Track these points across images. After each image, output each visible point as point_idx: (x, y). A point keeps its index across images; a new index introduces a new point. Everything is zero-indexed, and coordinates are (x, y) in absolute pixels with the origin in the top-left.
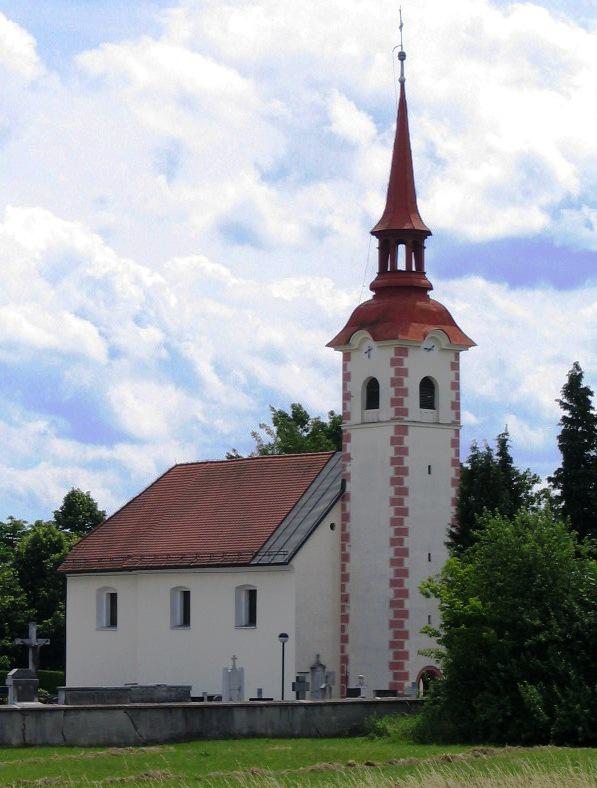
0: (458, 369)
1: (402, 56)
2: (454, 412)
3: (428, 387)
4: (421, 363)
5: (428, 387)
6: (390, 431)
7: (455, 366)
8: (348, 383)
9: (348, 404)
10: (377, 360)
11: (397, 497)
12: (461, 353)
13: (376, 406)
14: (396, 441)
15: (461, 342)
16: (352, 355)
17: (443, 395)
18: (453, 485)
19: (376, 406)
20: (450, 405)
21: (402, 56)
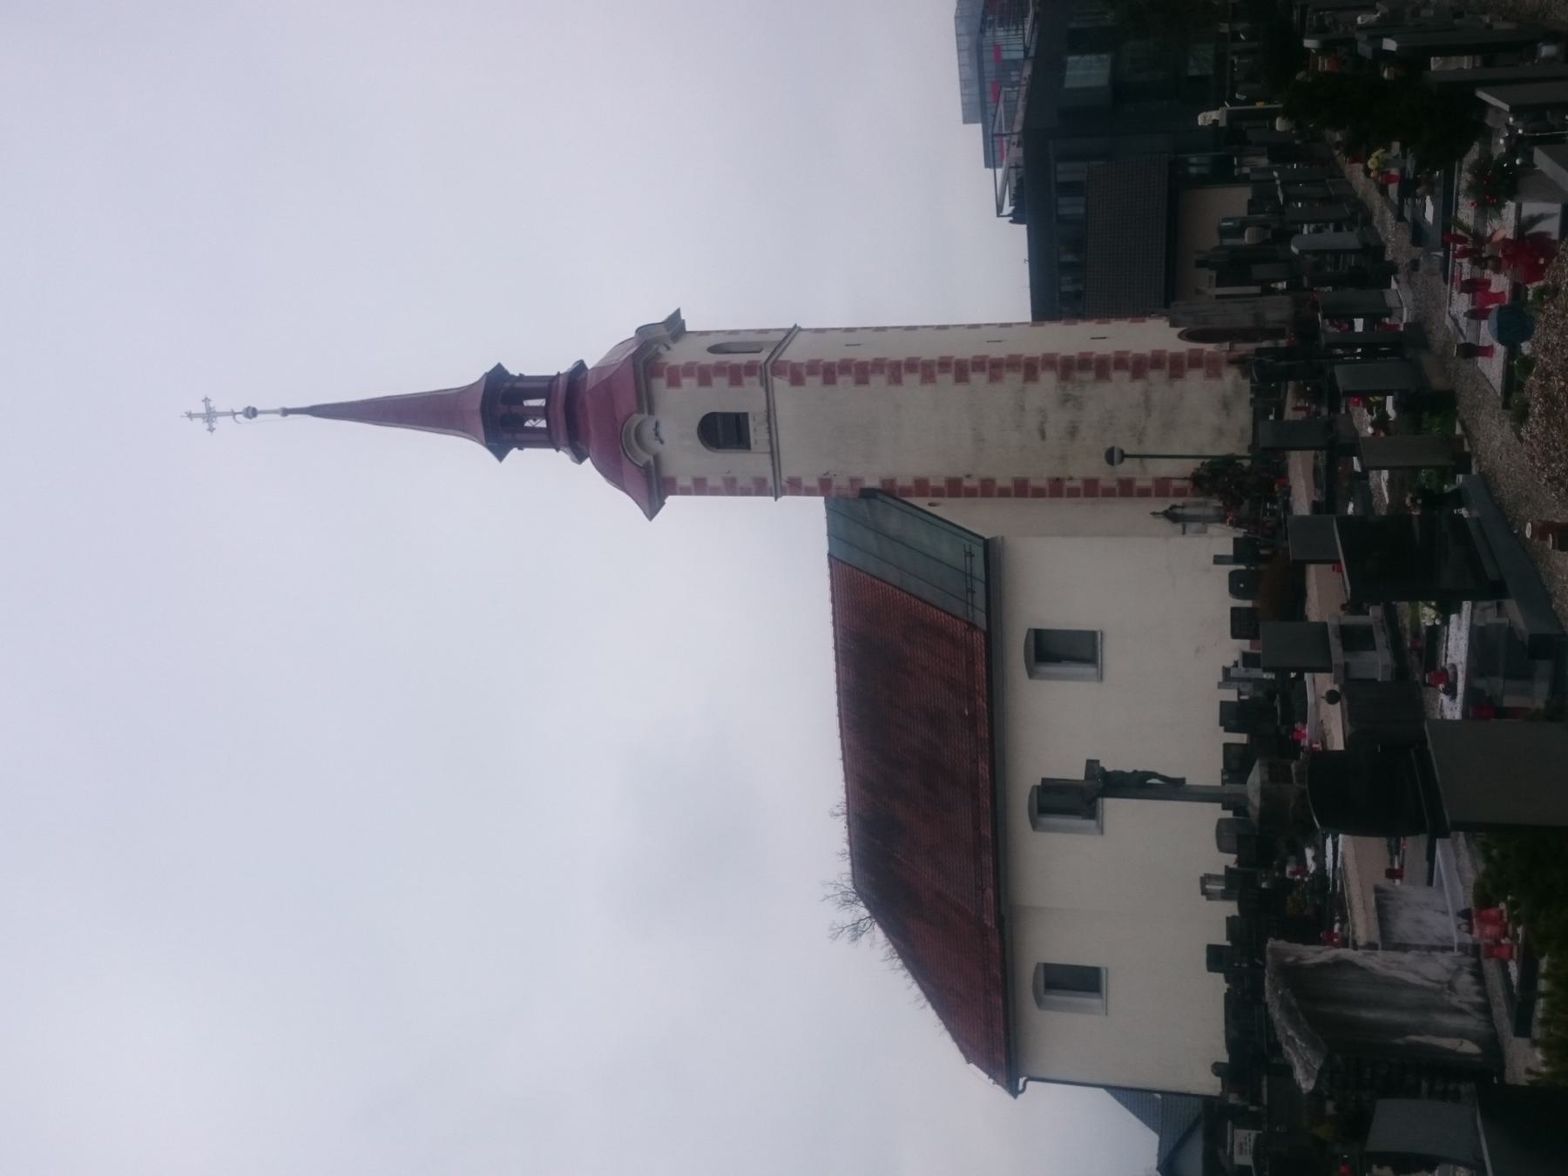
1: (251, 413)
6: (780, 384)
21: (251, 413)
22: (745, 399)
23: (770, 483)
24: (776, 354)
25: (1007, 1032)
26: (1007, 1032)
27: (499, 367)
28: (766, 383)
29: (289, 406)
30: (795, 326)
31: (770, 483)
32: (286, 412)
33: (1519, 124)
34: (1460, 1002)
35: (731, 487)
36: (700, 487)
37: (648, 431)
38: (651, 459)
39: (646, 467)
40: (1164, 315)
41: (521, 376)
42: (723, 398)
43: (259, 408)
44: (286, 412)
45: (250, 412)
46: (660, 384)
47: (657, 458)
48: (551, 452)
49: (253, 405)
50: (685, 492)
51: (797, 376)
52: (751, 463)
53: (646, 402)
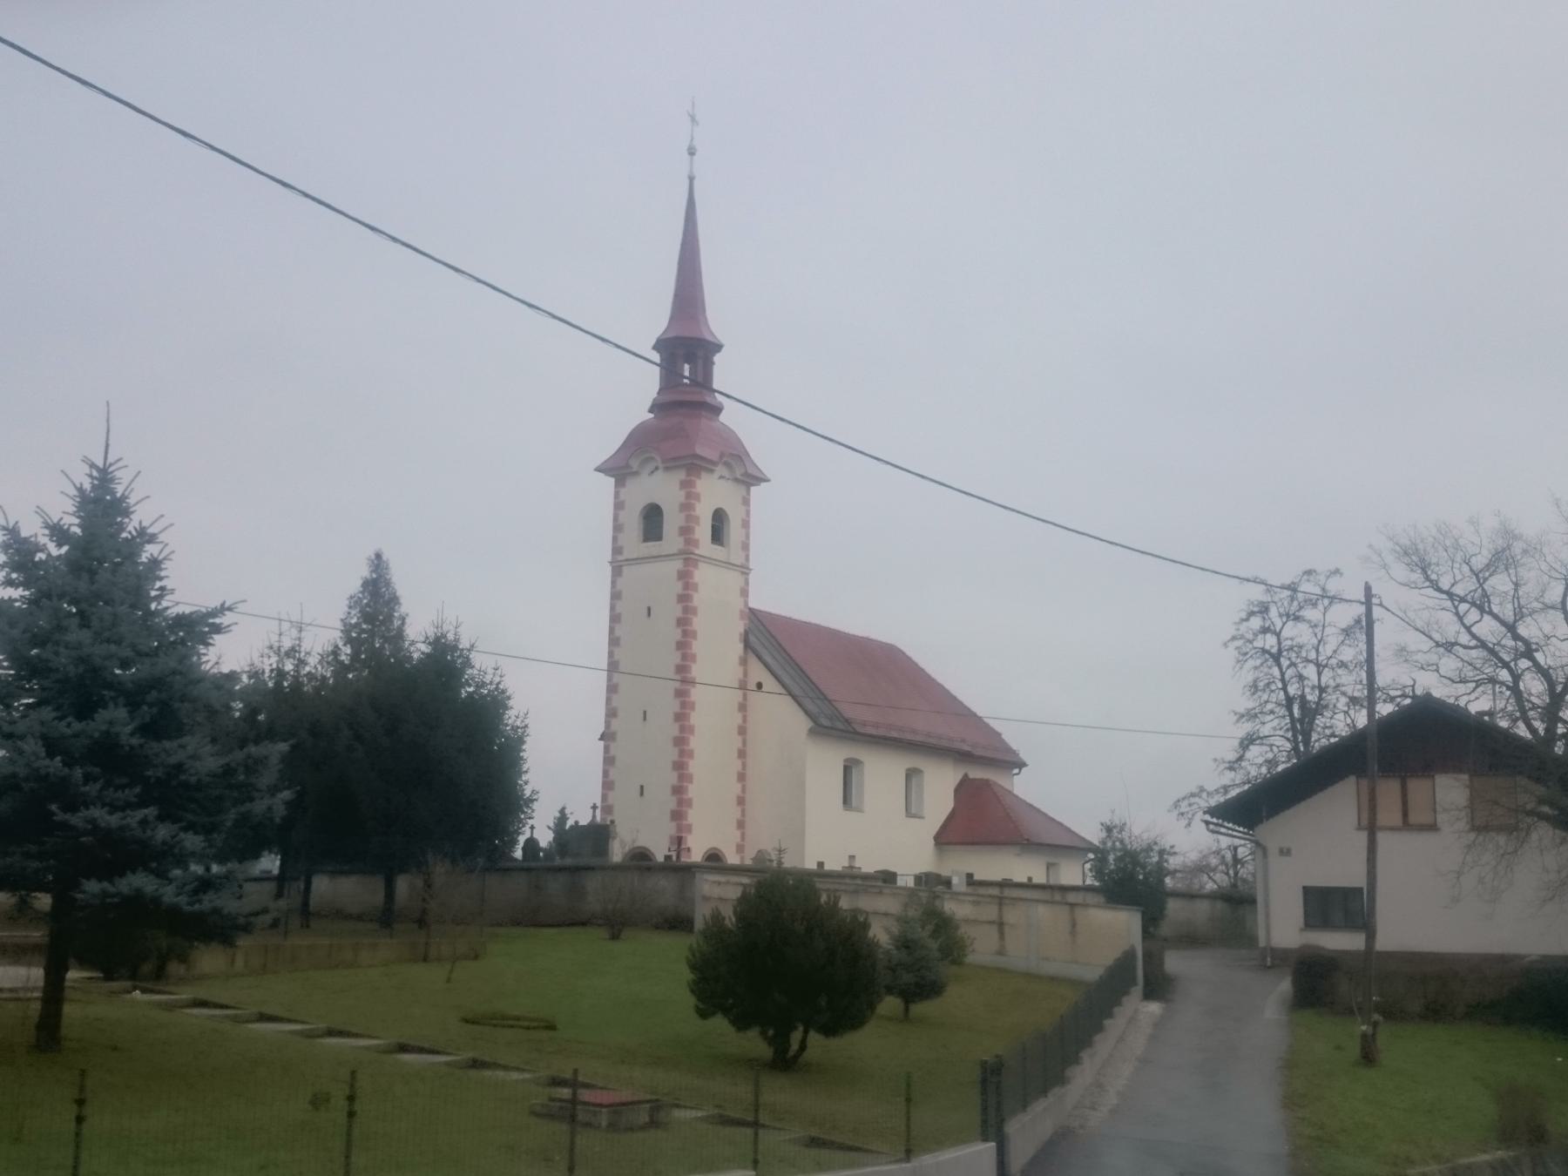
0: (747, 596)
1: (692, 152)
2: (744, 531)
3: (719, 518)
4: (713, 491)
5: (719, 518)
6: (678, 565)
7: (746, 501)
8: (615, 697)
9: (616, 651)
10: (661, 487)
11: (689, 478)
12: (752, 488)
13: (659, 538)
14: (684, 576)
15: (750, 478)
16: (625, 569)
17: (734, 531)
18: (742, 618)
19: (659, 538)
20: (736, 777)
21: (692, 152)
22: (671, 540)
23: (620, 558)
24: (702, 559)
25: (698, 867)
26: (698, 867)
27: (718, 347)
28: (681, 553)
29: (696, 182)
30: (751, 570)
31: (620, 558)
32: (691, 179)
33: (68, 609)
34: (183, 747)
35: (618, 528)
36: (619, 506)
37: (651, 466)
38: (634, 470)
39: (628, 466)
40: (866, 877)
41: (713, 363)
42: (672, 522)
43: (695, 157)
44: (691, 179)
45: (693, 151)
46: (681, 475)
47: (636, 473)
48: (656, 387)
49: (697, 153)
50: (617, 495)
51: (684, 576)
52: (633, 543)
53: (671, 464)
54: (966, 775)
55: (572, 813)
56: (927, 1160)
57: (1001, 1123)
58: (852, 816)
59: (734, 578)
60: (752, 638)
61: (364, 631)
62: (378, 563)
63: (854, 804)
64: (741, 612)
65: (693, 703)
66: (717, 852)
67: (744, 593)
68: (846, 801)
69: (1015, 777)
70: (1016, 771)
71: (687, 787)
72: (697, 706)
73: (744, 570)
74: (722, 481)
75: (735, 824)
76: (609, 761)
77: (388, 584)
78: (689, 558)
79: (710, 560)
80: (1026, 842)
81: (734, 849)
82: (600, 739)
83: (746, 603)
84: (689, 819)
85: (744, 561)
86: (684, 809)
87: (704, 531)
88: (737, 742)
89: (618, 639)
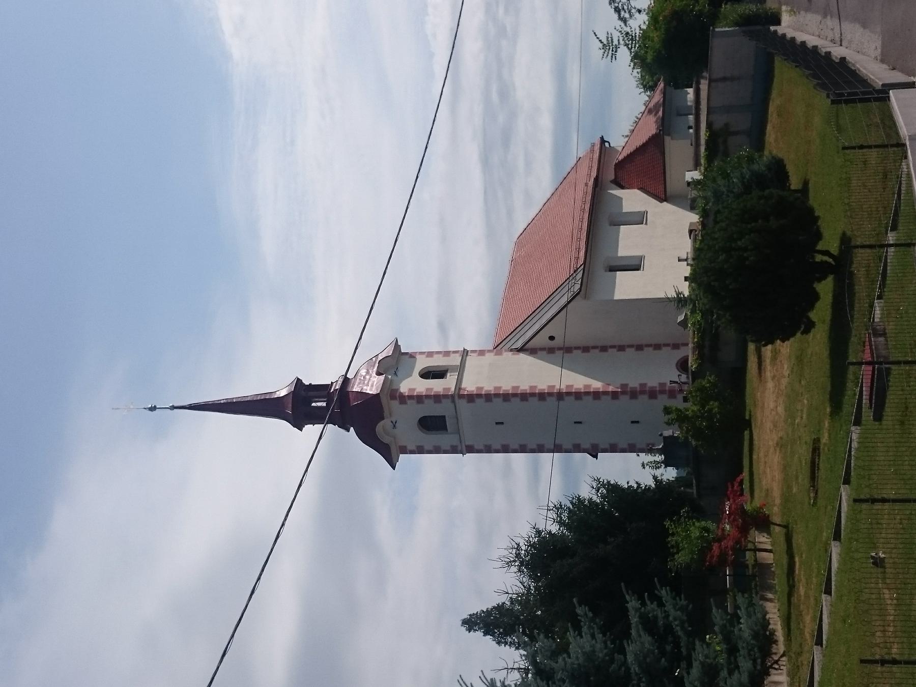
3: (427, 374)
5: (427, 374)
19: (443, 418)
21: (153, 409)
29: (176, 405)
54: (612, 182)
55: (628, 483)
56: (904, 131)
57: (878, 92)
58: (647, 263)
59: (471, 361)
60: (519, 344)
61: (524, 631)
62: (471, 623)
63: (637, 263)
64: (496, 354)
65: (660, 384)
66: (679, 364)
67: (482, 353)
68: (637, 268)
69: (611, 145)
70: (607, 145)
71: (630, 388)
72: (515, 385)
73: (465, 353)
74: (398, 373)
75: (639, 352)
76: (613, 449)
77: (488, 613)
78: (459, 396)
79: (459, 380)
80: (661, 132)
81: (676, 351)
82: (596, 456)
83: (489, 351)
84: (655, 385)
85: (457, 355)
86: (647, 389)
87: (437, 386)
88: (630, 352)
89: (486, 446)
